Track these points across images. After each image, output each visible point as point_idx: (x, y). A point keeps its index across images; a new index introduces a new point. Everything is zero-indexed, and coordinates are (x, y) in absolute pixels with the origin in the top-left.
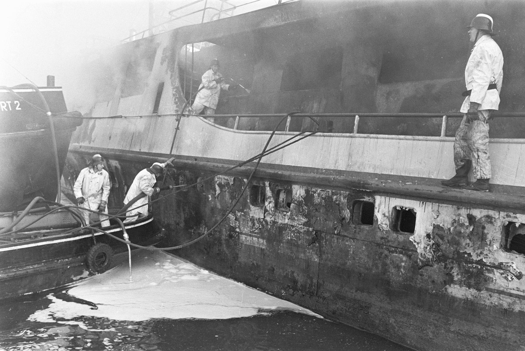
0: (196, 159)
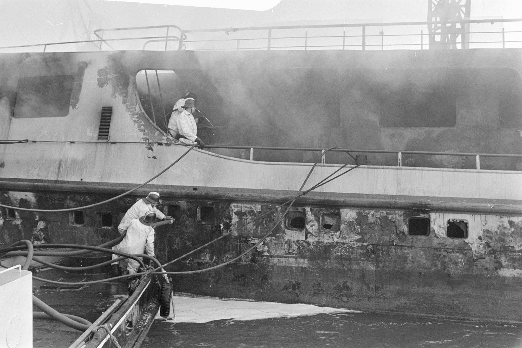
0: (195, 189)
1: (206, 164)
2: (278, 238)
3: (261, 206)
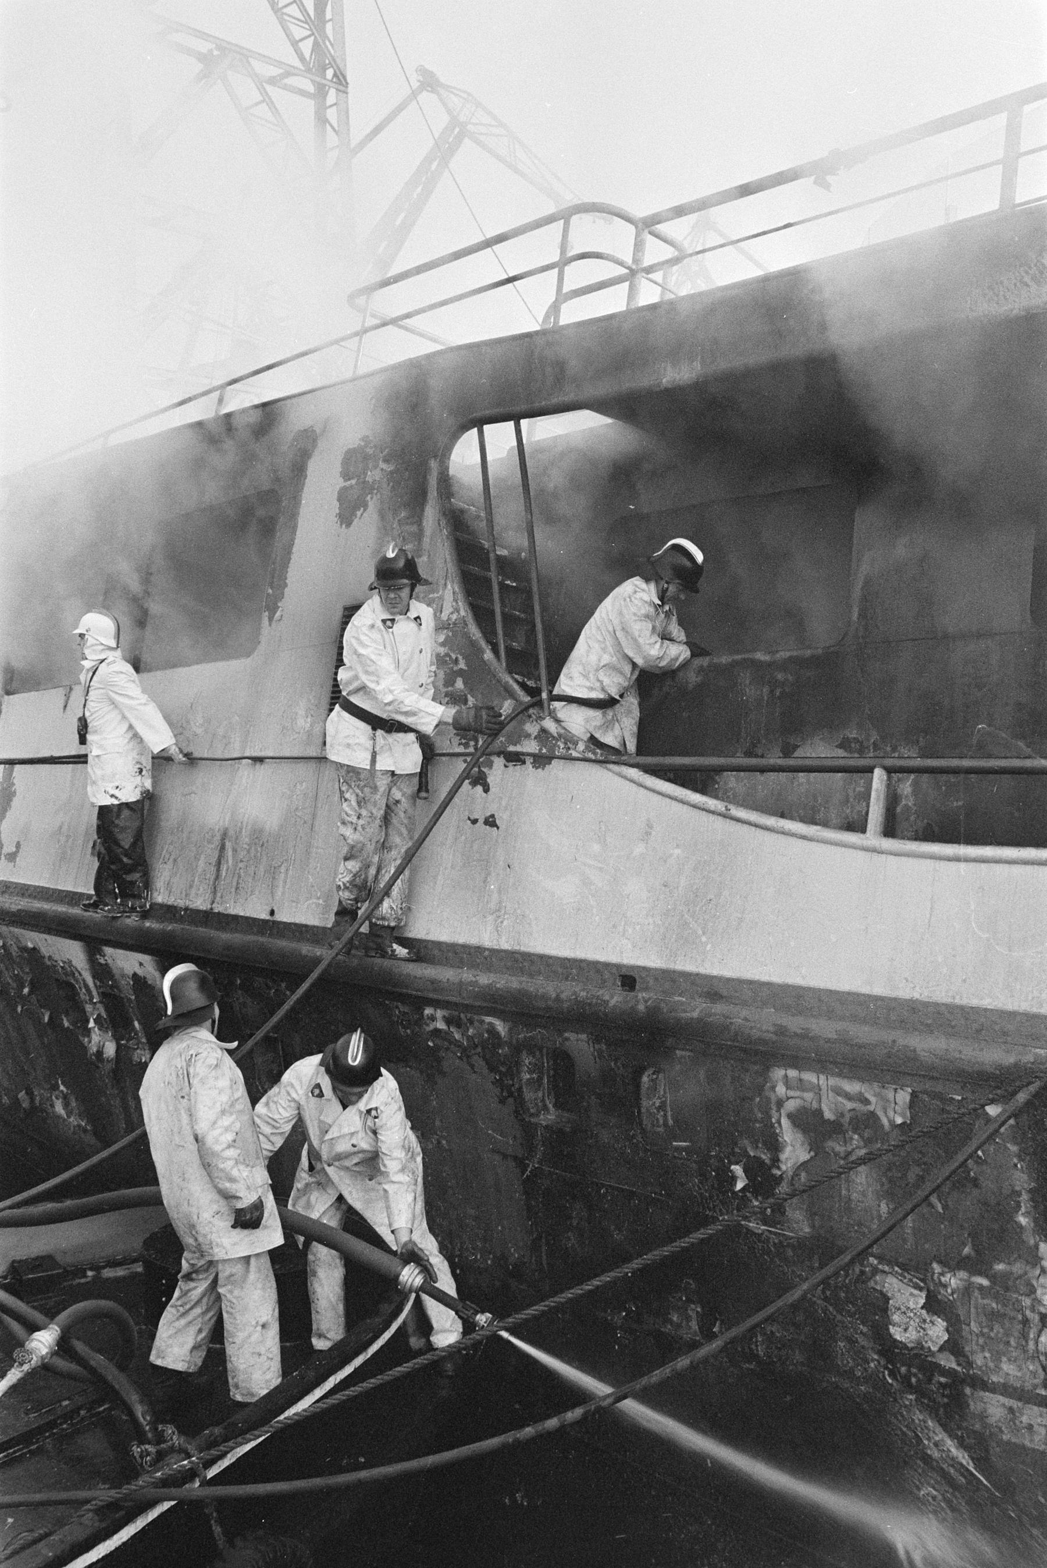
0: (629, 979)
1: (677, 851)
2: (1002, 1285)
3: (908, 1098)
